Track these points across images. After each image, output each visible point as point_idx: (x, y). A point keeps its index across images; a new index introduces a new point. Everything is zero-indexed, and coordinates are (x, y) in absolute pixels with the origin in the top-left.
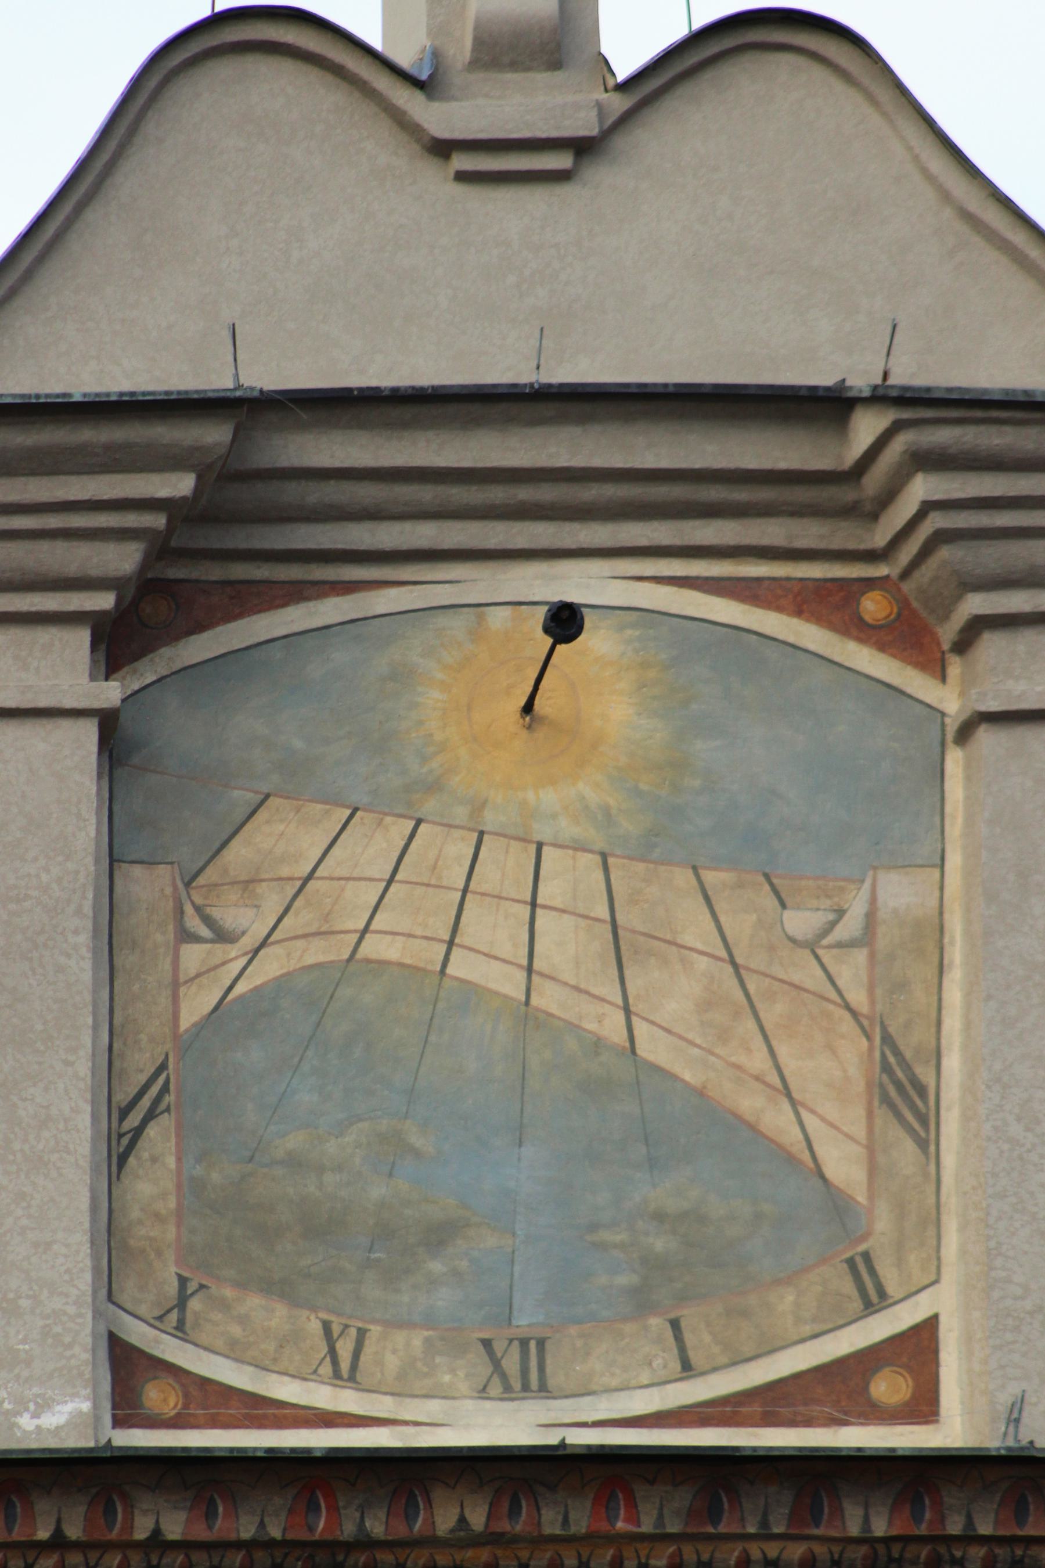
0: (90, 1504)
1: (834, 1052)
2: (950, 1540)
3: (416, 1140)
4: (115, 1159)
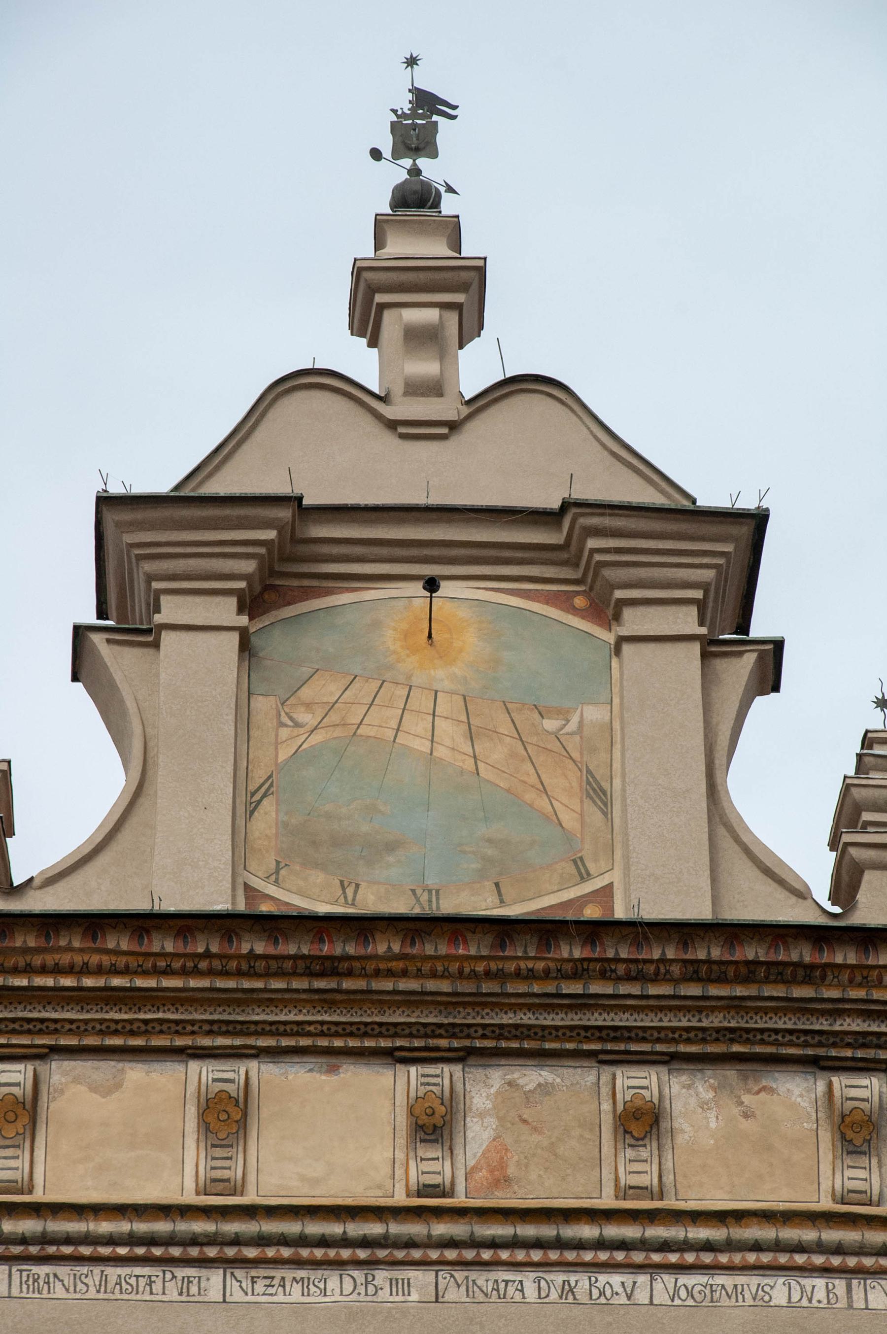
0: (222, 937)
1: (566, 777)
2: (608, 960)
3: (382, 808)
4: (248, 812)
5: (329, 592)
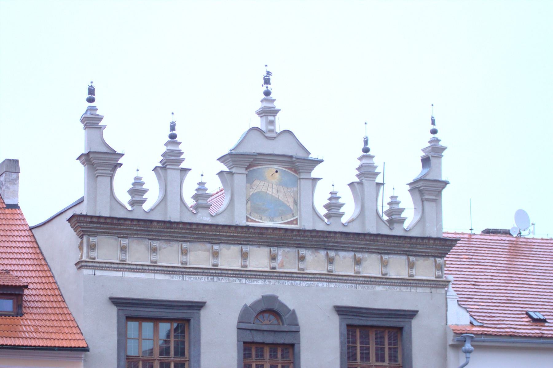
5: (258, 166)
